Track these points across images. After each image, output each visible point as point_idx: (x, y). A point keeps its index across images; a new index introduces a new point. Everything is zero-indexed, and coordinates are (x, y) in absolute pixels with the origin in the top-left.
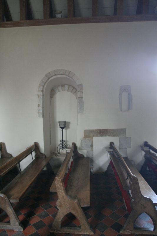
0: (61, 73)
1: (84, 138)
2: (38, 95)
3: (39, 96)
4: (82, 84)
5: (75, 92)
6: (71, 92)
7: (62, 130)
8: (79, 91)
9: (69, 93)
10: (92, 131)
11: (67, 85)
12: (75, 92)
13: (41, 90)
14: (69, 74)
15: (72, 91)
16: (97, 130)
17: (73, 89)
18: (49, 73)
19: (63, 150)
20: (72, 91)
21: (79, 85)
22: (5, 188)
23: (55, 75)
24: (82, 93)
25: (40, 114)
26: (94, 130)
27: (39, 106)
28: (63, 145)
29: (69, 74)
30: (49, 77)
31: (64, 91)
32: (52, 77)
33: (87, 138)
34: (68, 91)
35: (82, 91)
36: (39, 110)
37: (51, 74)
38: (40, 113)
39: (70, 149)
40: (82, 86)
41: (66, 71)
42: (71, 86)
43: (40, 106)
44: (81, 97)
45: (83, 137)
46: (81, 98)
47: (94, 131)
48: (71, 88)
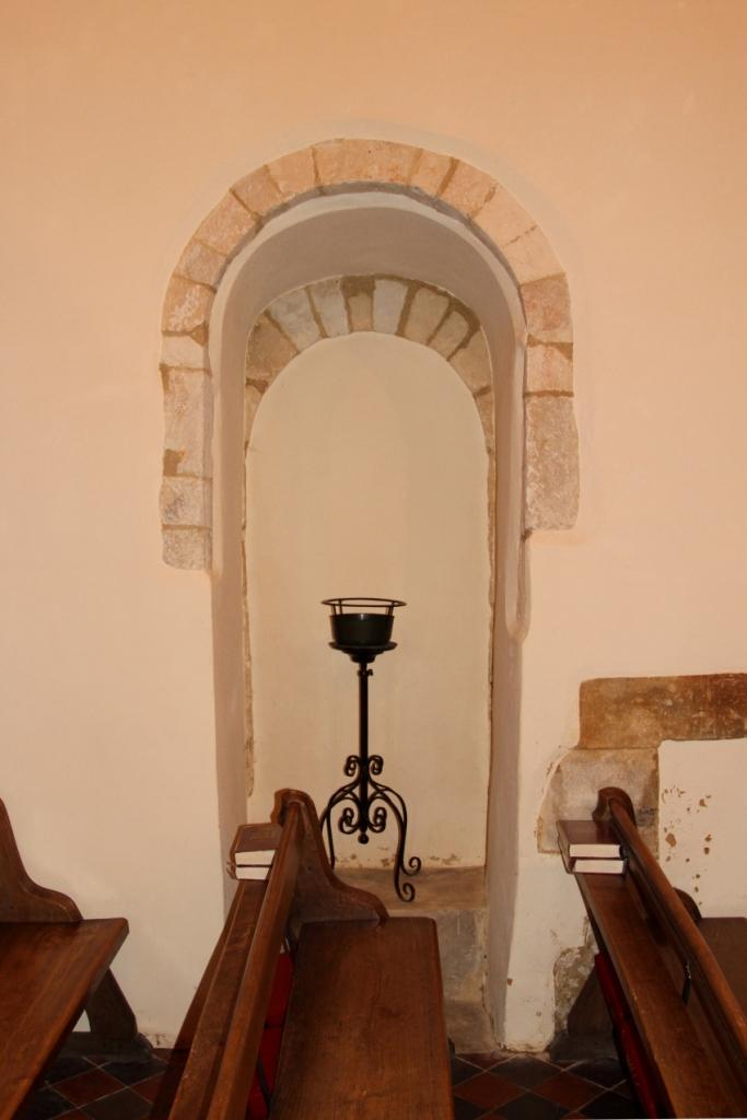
0: (375, 174)
1: (581, 747)
2: (165, 370)
3: (172, 374)
4: (560, 278)
5: (463, 345)
6: (429, 341)
7: (364, 675)
8: (532, 342)
9: (432, 358)
10: (647, 695)
11: (392, 278)
12: (463, 345)
13: (189, 327)
14: (444, 185)
15: (438, 328)
16: (696, 678)
17: (447, 315)
18: (266, 169)
19: (364, 840)
20: (438, 328)
21: (536, 285)
22: (687, 913)
23: (322, 191)
24: (557, 353)
25: (182, 534)
26: (669, 680)
27: (171, 463)
28: (363, 803)
29: (444, 185)
30: (263, 211)
31: (371, 328)
32: (285, 207)
33: (609, 754)
34: (401, 332)
35: (562, 337)
36: (172, 505)
37: (281, 185)
38: (183, 527)
39: (267, 856)
40: (563, 293)
41: (419, 154)
42: (433, 289)
43: (181, 467)
44: (556, 394)
45: (576, 744)
46: (551, 401)
47: (672, 688)
48: (428, 308)
